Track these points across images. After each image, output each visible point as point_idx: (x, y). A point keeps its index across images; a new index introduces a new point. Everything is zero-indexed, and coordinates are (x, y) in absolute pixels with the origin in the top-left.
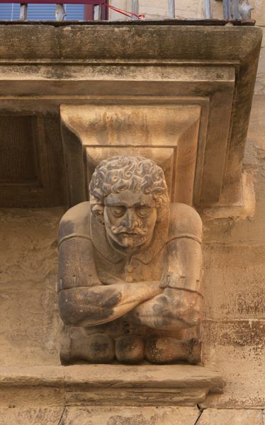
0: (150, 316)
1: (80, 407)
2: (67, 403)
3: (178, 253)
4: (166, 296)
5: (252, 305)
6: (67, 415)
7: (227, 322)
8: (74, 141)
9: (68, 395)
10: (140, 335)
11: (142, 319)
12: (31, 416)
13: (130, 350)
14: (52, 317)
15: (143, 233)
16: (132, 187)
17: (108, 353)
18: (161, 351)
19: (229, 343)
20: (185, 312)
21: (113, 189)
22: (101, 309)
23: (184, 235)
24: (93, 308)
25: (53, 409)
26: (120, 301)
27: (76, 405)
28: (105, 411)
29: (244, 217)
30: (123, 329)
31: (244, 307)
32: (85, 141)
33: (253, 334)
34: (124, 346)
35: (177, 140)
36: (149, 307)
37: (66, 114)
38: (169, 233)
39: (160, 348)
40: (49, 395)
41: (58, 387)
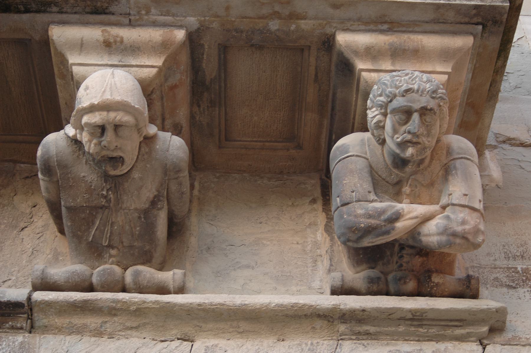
0: (433, 235)
1: (355, 341)
2: (340, 336)
3: (459, 172)
4: (450, 214)
5: (518, 254)
6: (340, 348)
7: (495, 268)
8: (346, 68)
9: (342, 328)
10: (413, 271)
11: (424, 239)
12: (302, 350)
13: (405, 283)
14: (316, 261)
15: (427, 142)
16: (418, 91)
17: (382, 286)
18: (437, 284)
19: (502, 285)
20: (470, 229)
21: (399, 92)
22: (384, 224)
23: (461, 156)
24: (373, 222)
25: (325, 342)
26: (403, 216)
27: (351, 339)
28: (382, 345)
29: (493, 185)
30: (397, 263)
31: (510, 255)
32: (360, 65)
33: (524, 278)
34: (401, 280)
35: (451, 68)
36: (432, 226)
37: (343, 39)
38: (447, 155)
39: (436, 282)
40: (321, 327)
41: (328, 318)
